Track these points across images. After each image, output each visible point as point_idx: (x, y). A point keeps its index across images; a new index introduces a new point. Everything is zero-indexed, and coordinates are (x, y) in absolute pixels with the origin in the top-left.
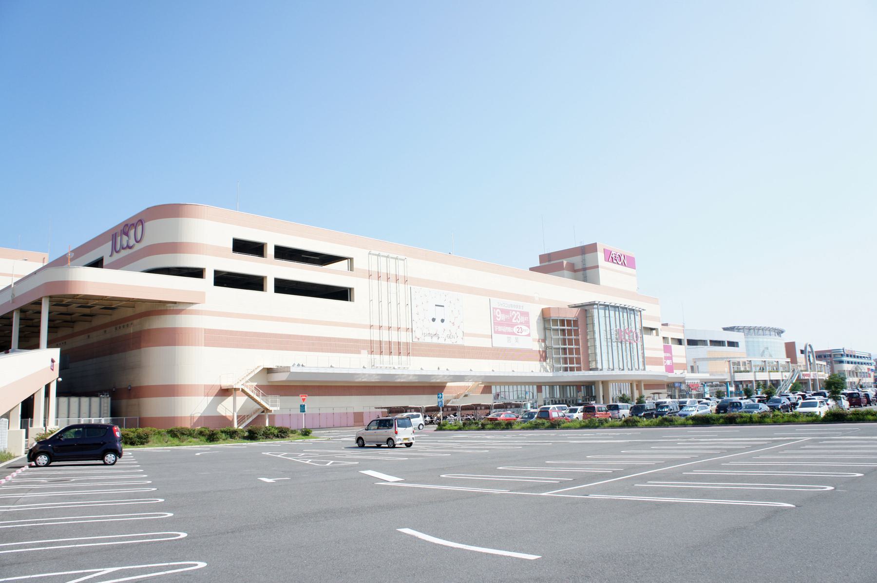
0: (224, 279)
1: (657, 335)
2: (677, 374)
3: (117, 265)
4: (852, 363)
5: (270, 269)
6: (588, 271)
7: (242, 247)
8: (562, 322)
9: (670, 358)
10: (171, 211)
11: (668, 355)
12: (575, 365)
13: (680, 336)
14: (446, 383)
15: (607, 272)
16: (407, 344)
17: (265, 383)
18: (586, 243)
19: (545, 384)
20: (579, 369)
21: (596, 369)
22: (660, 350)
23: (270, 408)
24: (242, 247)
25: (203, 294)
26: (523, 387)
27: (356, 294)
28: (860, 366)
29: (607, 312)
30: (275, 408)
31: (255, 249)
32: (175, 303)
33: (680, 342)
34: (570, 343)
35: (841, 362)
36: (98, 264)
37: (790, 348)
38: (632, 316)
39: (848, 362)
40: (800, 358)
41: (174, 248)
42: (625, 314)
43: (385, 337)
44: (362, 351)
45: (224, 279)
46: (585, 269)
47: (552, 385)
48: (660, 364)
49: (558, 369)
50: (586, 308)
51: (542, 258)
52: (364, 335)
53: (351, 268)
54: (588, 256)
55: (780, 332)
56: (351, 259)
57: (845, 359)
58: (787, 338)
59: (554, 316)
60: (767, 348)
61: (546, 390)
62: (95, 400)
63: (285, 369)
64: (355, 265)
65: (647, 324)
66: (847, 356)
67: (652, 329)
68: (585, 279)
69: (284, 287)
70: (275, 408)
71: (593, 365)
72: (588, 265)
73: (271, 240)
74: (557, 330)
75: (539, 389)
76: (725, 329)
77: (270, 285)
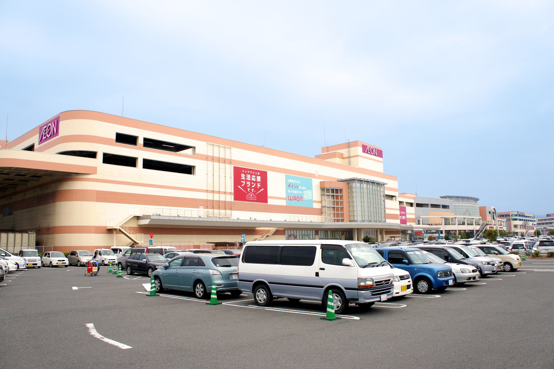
0: (109, 159)
1: (396, 200)
3: (41, 150)
5: (141, 153)
7: (122, 138)
8: (333, 191)
11: (403, 213)
12: (340, 218)
13: (412, 201)
20: (343, 220)
21: (354, 221)
24: (122, 138)
27: (197, 170)
31: (130, 140)
33: (411, 205)
36: (31, 148)
45: (109, 159)
48: (398, 219)
55: (476, 200)
56: (194, 148)
58: (480, 204)
59: (327, 186)
62: (25, 235)
66: (520, 216)
67: (393, 196)
69: (149, 164)
72: (351, 155)
73: (141, 134)
74: (329, 195)
76: (441, 197)
77: (140, 163)
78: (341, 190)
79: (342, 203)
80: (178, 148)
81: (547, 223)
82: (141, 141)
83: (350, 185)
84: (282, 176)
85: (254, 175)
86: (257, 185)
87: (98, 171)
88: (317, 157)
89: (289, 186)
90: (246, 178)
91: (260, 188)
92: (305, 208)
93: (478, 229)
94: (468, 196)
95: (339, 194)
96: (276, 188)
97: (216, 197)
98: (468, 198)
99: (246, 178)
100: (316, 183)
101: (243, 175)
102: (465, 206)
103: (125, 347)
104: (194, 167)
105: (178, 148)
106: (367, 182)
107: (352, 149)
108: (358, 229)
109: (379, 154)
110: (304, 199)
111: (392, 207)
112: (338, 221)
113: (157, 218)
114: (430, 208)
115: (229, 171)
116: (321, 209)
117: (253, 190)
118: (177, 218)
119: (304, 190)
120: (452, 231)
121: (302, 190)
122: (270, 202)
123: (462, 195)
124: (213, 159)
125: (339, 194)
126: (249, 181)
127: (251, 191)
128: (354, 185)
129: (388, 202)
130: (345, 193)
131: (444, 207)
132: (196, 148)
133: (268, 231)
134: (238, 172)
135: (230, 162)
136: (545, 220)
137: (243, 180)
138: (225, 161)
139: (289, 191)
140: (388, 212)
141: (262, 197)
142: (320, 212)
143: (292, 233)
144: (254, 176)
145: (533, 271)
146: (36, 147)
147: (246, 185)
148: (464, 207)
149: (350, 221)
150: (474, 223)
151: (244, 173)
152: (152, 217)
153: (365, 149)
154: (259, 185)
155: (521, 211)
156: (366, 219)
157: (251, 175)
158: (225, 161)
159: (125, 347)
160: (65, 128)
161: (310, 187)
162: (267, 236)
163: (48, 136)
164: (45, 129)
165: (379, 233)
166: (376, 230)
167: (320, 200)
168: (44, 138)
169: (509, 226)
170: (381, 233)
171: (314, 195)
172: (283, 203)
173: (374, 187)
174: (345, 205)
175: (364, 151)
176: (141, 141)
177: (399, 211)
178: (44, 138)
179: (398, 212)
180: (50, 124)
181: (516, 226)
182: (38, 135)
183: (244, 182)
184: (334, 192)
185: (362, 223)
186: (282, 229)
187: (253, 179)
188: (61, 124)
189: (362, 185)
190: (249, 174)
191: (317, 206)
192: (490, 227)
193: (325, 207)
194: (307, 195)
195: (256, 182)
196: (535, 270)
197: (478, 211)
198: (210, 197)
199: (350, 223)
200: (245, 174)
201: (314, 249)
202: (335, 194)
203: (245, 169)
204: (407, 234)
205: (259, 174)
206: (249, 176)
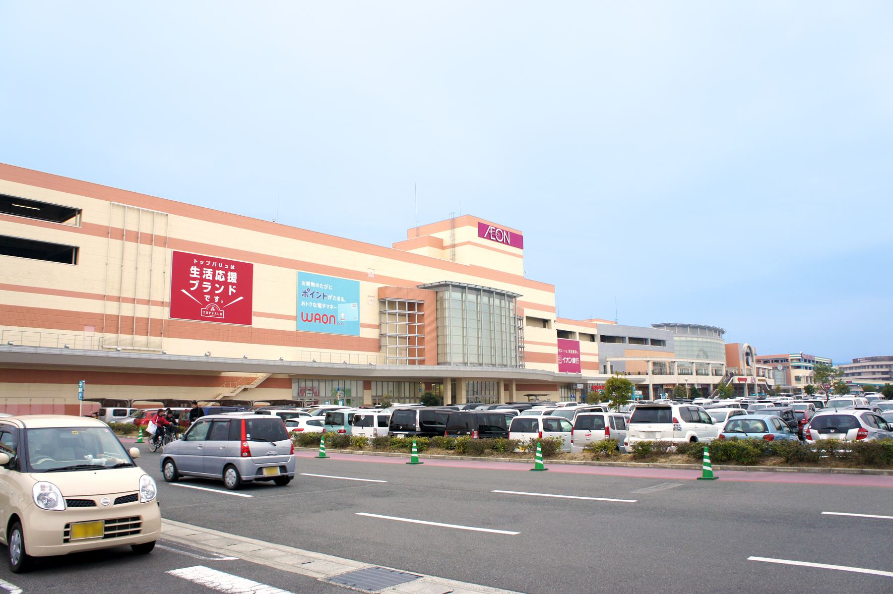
6: (457, 249)
8: (402, 305)
12: (417, 358)
13: (593, 331)
20: (422, 362)
21: (445, 363)
22: (162, 304)
33: (592, 338)
44: (86, 327)
48: (553, 362)
55: (720, 332)
58: (726, 339)
59: (391, 297)
66: (805, 361)
72: (457, 242)
74: (404, 315)
76: (653, 326)
78: (420, 305)
79: (421, 329)
80: (59, 214)
81: (853, 374)
83: (440, 295)
84: (291, 274)
85: (223, 269)
86: (226, 290)
89: (305, 293)
90: (201, 274)
91: (235, 296)
92: (341, 338)
93: (716, 382)
94: (703, 324)
95: (416, 312)
97: (127, 310)
98: (710, 329)
99: (201, 274)
100: (369, 291)
101: (194, 271)
102: (698, 342)
103: (752, 558)
104: (77, 249)
105: (59, 214)
106: (477, 290)
107: (458, 231)
108: (505, 380)
109: (516, 240)
110: (339, 319)
111: (542, 340)
112: (412, 362)
114: (627, 345)
115: (164, 259)
116: (379, 340)
117: (217, 298)
119: (340, 302)
120: (667, 385)
121: (335, 303)
123: (692, 323)
124: (121, 234)
125: (416, 312)
126: (208, 281)
127: (212, 300)
128: (447, 295)
129: (531, 333)
130: (428, 311)
131: (655, 342)
132: (83, 213)
133: (249, 380)
134: (182, 263)
135: (163, 242)
136: (851, 368)
138: (150, 239)
139: (303, 303)
140: (528, 348)
142: (377, 346)
143: (341, 387)
147: (200, 287)
148: (695, 344)
149: (438, 364)
150: (694, 373)
151: (198, 265)
153: (483, 230)
154: (231, 290)
155: (808, 352)
156: (487, 360)
157: (215, 269)
158: (150, 239)
159: (752, 558)
161: (354, 297)
162: (245, 389)
165: (502, 388)
166: (498, 381)
167: (377, 323)
169: (788, 381)
170: (507, 387)
171: (364, 312)
172: (290, 326)
173: (503, 302)
174: (429, 334)
175: (481, 235)
177: (556, 348)
179: (555, 350)
181: (798, 379)
183: (197, 283)
184: (411, 309)
185: (462, 368)
186: (286, 377)
189: (479, 297)
190: (209, 267)
191: (373, 334)
192: (739, 379)
194: (346, 312)
195: (226, 284)
197: (724, 351)
198: (111, 309)
199: (437, 368)
201: (372, 417)
203: (200, 258)
204: (576, 390)
205: (233, 267)
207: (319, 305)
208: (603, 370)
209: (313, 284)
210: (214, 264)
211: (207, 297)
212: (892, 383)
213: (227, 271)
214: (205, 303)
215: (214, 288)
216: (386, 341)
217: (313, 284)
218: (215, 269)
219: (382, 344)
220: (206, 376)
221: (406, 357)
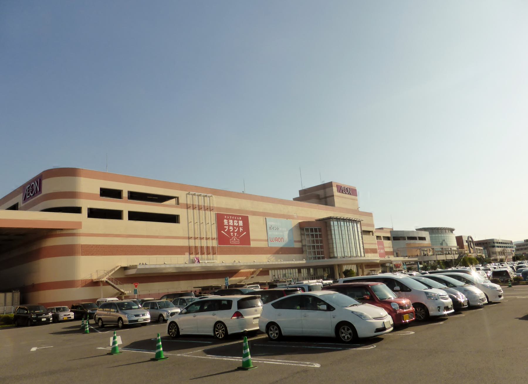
0: (93, 213)
1: (373, 235)
2: (386, 258)
3: (26, 208)
4: (500, 247)
5: (126, 206)
6: (328, 199)
7: (106, 193)
8: (312, 230)
9: (383, 248)
10: (71, 172)
11: (381, 247)
14: (240, 270)
15: (339, 199)
16: (213, 247)
17: (122, 276)
18: (326, 182)
19: (304, 267)
20: (323, 258)
21: (334, 257)
23: (125, 292)
24: (106, 193)
25: (79, 224)
26: (289, 270)
27: (181, 219)
28: (506, 249)
29: (345, 223)
30: (128, 292)
31: (116, 194)
32: (62, 229)
33: (388, 238)
34: (317, 242)
35: (494, 247)
36: (15, 207)
37: (459, 239)
38: (355, 224)
39: (498, 247)
40: (465, 244)
41: (73, 195)
42: (351, 224)
43: (198, 243)
45: (93, 213)
46: (326, 198)
47: (308, 268)
49: (310, 259)
50: (326, 221)
51: (301, 192)
52: (184, 243)
53: (178, 203)
54: (328, 190)
55: (452, 230)
56: (178, 198)
57: (496, 245)
58: (456, 233)
60: (444, 240)
61: (304, 272)
62: (9, 295)
63: (134, 267)
64: (180, 201)
65: (364, 228)
66: (497, 243)
67: (369, 232)
68: (326, 204)
69: (134, 216)
70: (128, 292)
71: (332, 256)
72: (327, 195)
73: (126, 188)
74: (309, 235)
75: (299, 272)
77: (126, 215)
82: (125, 195)
85: (237, 220)
86: (239, 230)
87: (83, 226)
88: (295, 199)
90: (228, 223)
91: (243, 232)
95: (318, 233)
96: (257, 232)
99: (228, 223)
101: (225, 221)
112: (319, 258)
113: (143, 267)
115: (211, 217)
116: (302, 248)
117: (236, 234)
118: (163, 266)
122: (253, 244)
126: (231, 226)
127: (234, 235)
134: (220, 218)
137: (226, 226)
141: (246, 240)
144: (236, 221)
145: (516, 299)
146: (21, 205)
147: (229, 230)
152: (139, 267)
154: (241, 229)
157: (233, 220)
160: (49, 186)
163: (31, 195)
164: (29, 188)
168: (28, 197)
176: (125, 195)
178: (28, 197)
180: (33, 183)
182: (22, 194)
183: (227, 227)
187: (236, 224)
188: (44, 182)
190: (231, 219)
193: (305, 246)
195: (238, 227)
196: (518, 297)
200: (228, 219)
202: (314, 233)
203: (227, 215)
205: (240, 218)
206: (231, 221)
207: (277, 233)
208: (395, 255)
209: (273, 223)
210: (233, 217)
211: (232, 233)
212: (527, 253)
213: (238, 220)
214: (231, 237)
215: (234, 230)
216: (306, 249)
217: (273, 223)
218: (233, 220)
219: (304, 249)
220: (231, 272)
221: (313, 255)
